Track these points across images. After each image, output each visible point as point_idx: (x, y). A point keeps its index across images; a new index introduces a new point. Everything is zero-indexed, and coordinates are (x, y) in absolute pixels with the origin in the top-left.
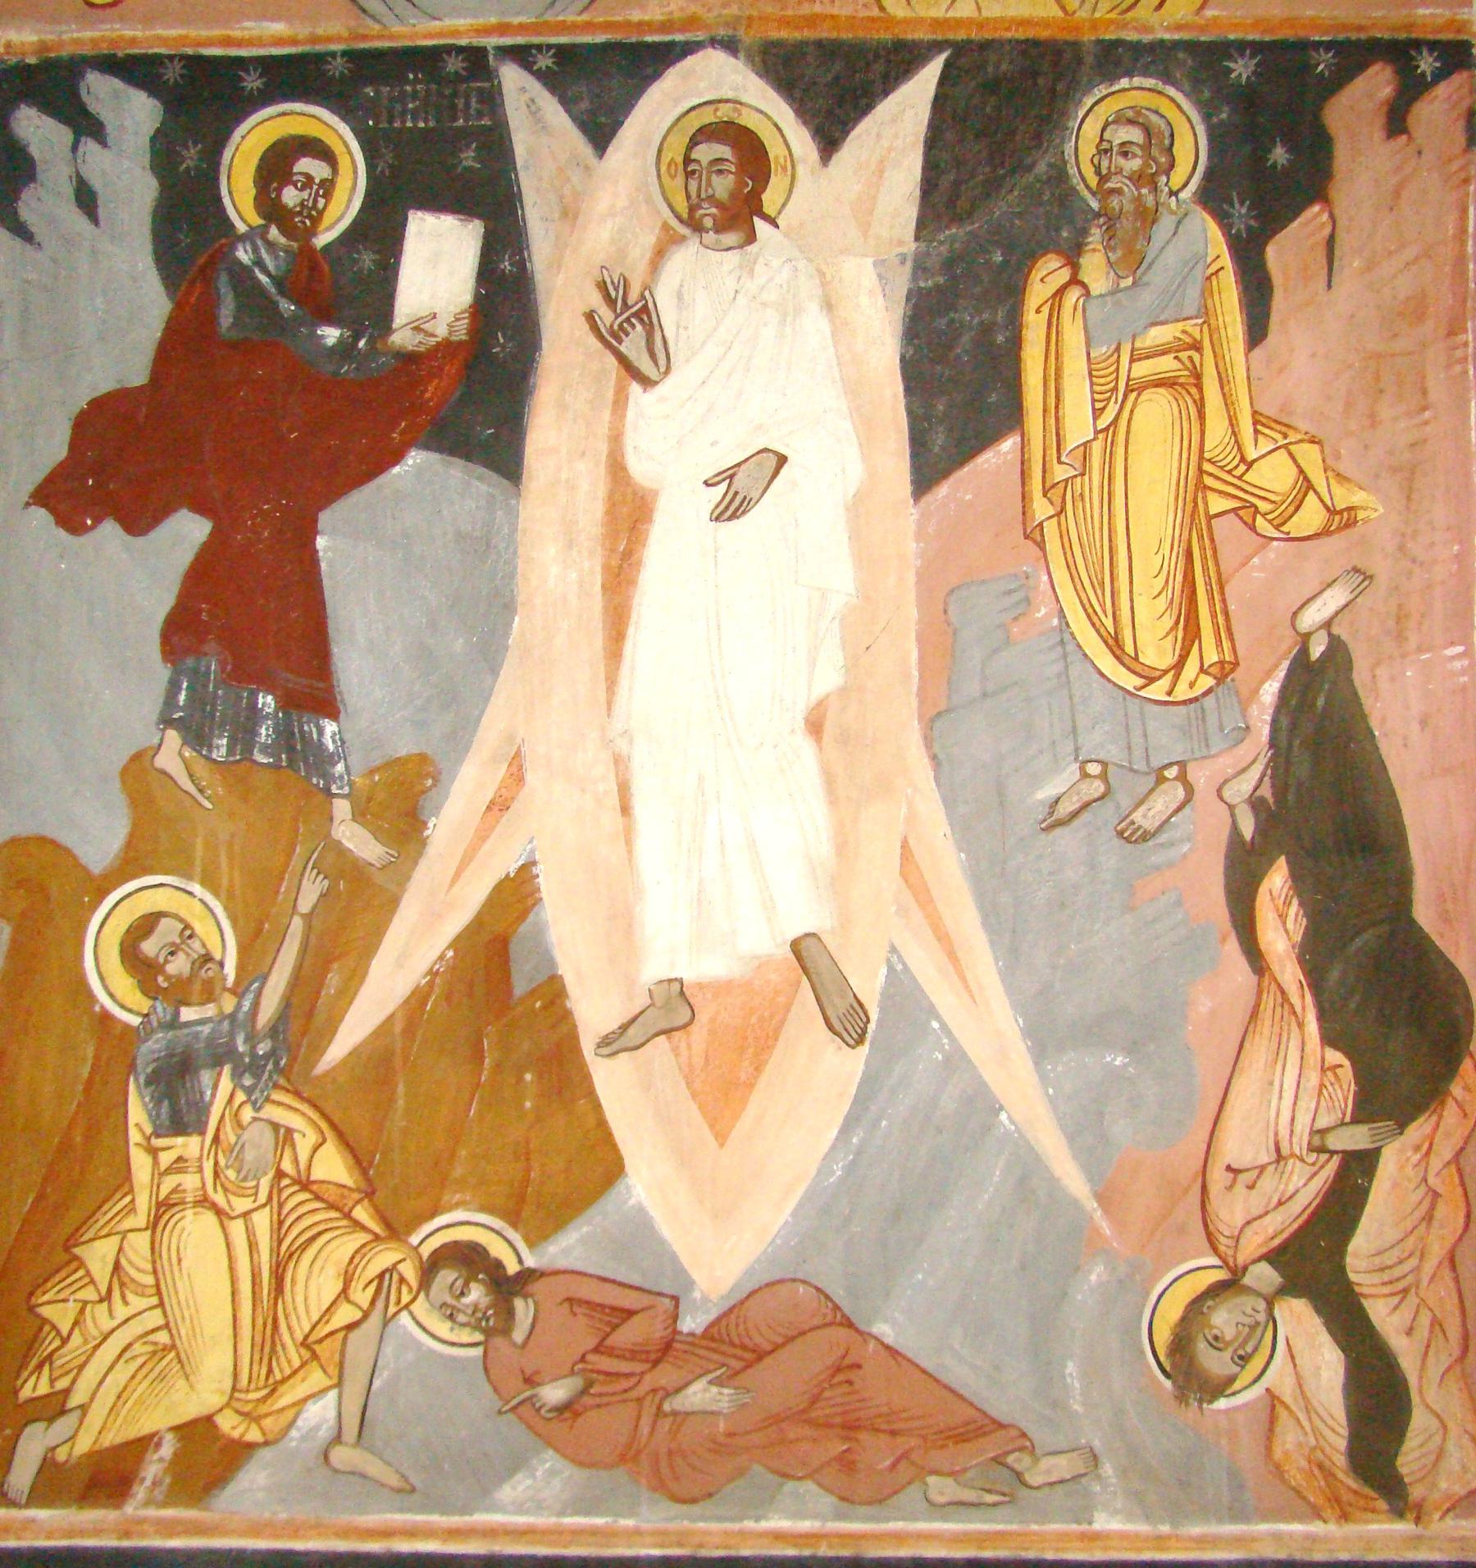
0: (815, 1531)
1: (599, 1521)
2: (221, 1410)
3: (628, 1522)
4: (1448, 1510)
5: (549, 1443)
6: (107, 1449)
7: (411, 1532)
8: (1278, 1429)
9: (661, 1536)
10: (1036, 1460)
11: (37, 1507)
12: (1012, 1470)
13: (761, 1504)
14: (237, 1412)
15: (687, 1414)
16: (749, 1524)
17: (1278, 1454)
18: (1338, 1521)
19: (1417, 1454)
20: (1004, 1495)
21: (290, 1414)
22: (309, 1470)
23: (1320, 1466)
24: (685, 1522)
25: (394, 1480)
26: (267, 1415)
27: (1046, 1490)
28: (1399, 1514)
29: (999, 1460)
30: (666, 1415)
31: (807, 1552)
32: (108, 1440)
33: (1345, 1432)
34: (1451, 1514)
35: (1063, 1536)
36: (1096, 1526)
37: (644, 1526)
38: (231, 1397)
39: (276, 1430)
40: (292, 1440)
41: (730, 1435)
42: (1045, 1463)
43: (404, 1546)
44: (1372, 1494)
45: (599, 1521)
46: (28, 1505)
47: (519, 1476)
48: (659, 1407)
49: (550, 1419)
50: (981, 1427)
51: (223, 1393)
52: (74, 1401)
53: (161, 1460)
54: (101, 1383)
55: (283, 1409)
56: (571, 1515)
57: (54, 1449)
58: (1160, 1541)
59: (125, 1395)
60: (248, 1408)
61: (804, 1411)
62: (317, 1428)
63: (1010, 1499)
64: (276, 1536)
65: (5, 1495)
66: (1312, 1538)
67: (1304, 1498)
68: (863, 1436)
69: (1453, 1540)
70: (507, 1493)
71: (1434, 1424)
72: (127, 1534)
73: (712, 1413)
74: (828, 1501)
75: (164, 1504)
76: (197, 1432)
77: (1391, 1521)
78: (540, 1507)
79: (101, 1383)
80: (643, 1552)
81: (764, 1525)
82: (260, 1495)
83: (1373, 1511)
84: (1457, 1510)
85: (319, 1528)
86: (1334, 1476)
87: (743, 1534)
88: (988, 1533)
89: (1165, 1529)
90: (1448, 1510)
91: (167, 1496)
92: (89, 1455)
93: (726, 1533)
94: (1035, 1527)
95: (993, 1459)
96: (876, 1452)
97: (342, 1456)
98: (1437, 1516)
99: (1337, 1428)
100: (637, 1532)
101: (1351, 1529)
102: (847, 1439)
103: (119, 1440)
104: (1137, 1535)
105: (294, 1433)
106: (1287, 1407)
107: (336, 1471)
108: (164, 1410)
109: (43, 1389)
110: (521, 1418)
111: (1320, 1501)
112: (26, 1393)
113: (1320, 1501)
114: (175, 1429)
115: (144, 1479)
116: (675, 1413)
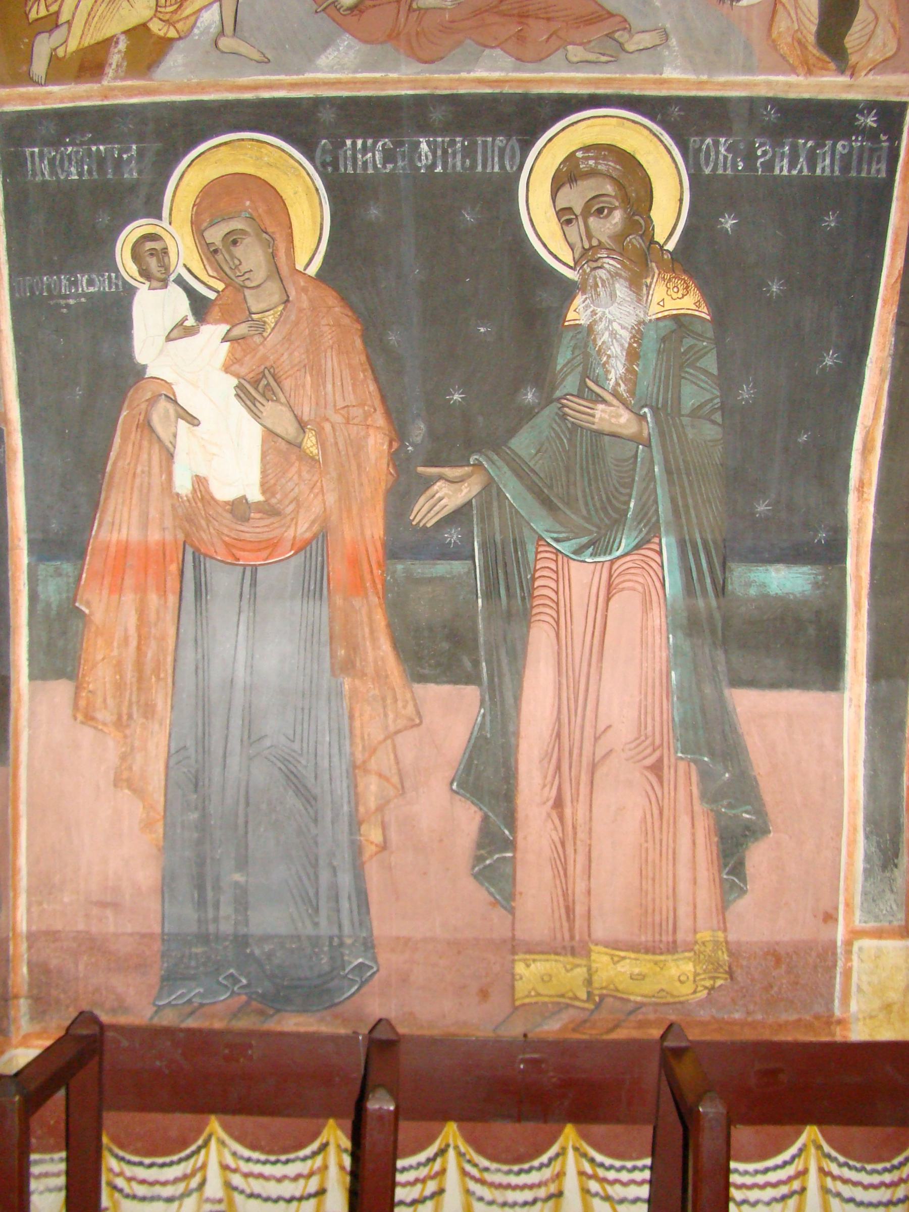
0: (198, 1042)
1: (378, 75)
2: (151, 19)
3: (393, 76)
4: (871, 70)
5: (347, 30)
6: (86, 48)
7: (270, 86)
8: (777, 19)
9: (413, 83)
10: (631, 36)
11: (52, 85)
12: (617, 42)
13: (472, 61)
14: (161, 20)
15: (427, 9)
16: (464, 75)
17: (774, 36)
18: (805, 75)
19: (856, 36)
20: (612, 56)
21: (193, 19)
22: (207, 52)
23: (799, 42)
24: (427, 75)
25: (256, 56)
26: (178, 21)
27: (636, 54)
28: (842, 72)
29: (610, 36)
30: (414, 10)
31: (497, 91)
32: (87, 42)
33: (817, 22)
34: (872, 72)
35: (645, 81)
36: (664, 76)
37: (404, 77)
38: (156, 11)
39: (185, 29)
40: (195, 35)
41: (453, 22)
42: (637, 38)
43: (266, 95)
44: (828, 59)
45: (378, 75)
46: (45, 85)
47: (329, 51)
48: (410, 6)
49: (345, 15)
50: (599, 16)
51: (151, 8)
52: (63, 18)
53: (119, 52)
54: (77, 7)
55: (187, 17)
56: (361, 72)
57: (55, 50)
58: (700, 84)
59: (93, 14)
60: (167, 17)
61: (496, 7)
62: (209, 27)
63: (615, 60)
64: (191, 93)
65: (32, 79)
66: (790, 85)
67: (787, 61)
68: (531, 22)
69: (869, 87)
70: (323, 61)
71: (871, 17)
72: (106, 97)
73: (440, 8)
74: (509, 61)
75: (123, 79)
76: (138, 33)
77: (836, 76)
78: (343, 68)
79: (77, 7)
80: (403, 93)
81: (472, 75)
82: (180, 69)
83: (826, 70)
84: (876, 70)
85: (216, 87)
86: (807, 49)
87: (462, 81)
88: (602, 79)
89: (704, 78)
90: (871, 70)
91: (126, 73)
92: (77, 52)
93: (451, 80)
94: (628, 76)
95: (607, 35)
96: (538, 30)
97: (226, 43)
98: (863, 73)
99: (812, 18)
100: (399, 81)
101: (812, 80)
102: (520, 23)
103: (92, 42)
104: (687, 81)
105: (196, 31)
106: (784, 5)
107: (223, 52)
108: (115, 24)
109: (43, 12)
110: (329, 15)
111: (796, 63)
112: (33, 15)
113: (796, 63)
114: (124, 33)
115: (111, 65)
116: (419, 9)
